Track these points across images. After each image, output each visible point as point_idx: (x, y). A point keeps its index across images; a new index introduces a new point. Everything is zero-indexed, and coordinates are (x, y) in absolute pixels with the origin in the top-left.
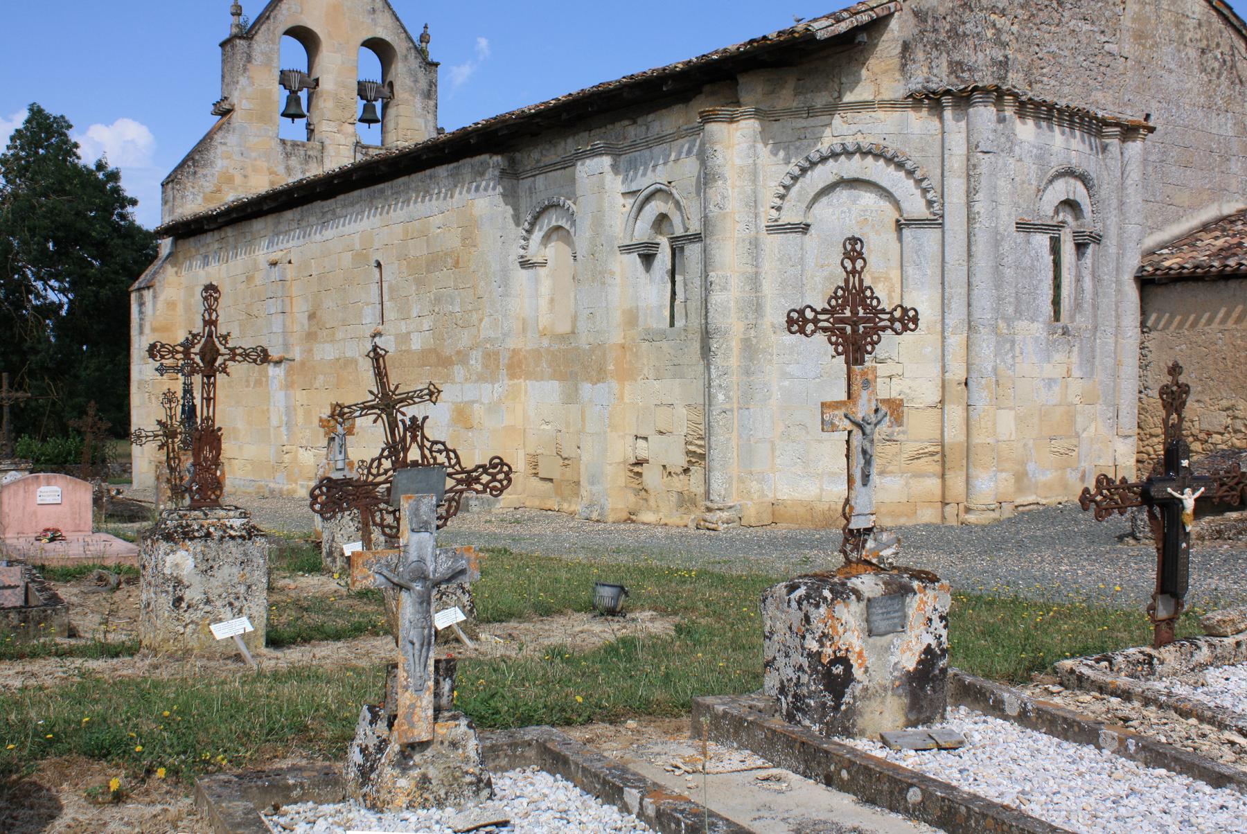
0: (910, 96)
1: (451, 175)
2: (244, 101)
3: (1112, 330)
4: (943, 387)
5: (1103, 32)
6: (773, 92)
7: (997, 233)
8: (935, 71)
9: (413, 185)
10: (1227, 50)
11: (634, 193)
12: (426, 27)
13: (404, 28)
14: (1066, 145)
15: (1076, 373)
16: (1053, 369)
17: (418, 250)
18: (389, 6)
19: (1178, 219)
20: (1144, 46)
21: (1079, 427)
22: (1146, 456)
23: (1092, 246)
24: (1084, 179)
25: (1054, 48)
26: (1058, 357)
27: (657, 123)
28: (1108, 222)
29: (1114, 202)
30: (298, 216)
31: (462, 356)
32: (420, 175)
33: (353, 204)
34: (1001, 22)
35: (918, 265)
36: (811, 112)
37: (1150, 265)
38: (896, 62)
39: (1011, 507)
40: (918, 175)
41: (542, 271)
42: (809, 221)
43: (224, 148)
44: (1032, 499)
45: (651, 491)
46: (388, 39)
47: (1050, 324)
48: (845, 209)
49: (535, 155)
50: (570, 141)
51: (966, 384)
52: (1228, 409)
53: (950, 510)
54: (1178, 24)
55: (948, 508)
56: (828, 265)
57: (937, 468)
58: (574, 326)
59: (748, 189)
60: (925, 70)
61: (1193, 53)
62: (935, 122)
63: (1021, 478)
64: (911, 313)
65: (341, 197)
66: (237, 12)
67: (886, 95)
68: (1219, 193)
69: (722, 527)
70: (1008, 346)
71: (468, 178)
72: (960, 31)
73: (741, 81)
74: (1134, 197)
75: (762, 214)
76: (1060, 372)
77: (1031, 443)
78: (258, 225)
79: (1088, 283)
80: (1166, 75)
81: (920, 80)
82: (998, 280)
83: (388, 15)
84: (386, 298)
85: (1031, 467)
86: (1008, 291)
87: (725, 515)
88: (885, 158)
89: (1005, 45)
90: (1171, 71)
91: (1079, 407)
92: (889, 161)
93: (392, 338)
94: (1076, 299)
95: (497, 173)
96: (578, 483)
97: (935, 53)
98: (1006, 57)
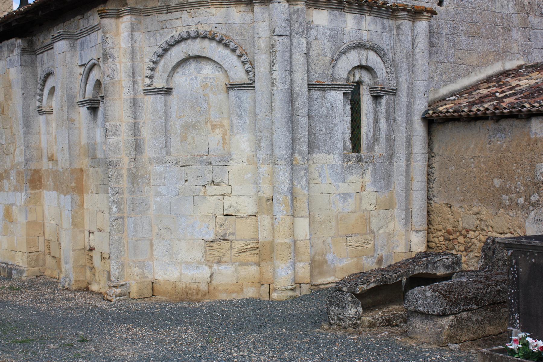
11: (84, 65)
15: (370, 188)
26: (351, 178)
28: (401, 80)
29: (404, 66)
35: (240, 116)
40: (238, 51)
41: (50, 117)
42: (171, 86)
45: (97, 269)
48: (193, 77)
51: (273, 200)
52: (477, 214)
56: (184, 117)
59: (129, 64)
68: (503, 54)
71: (6, 54)
75: (140, 82)
77: (329, 240)
79: (383, 124)
86: (303, 134)
87: (118, 291)
92: (220, 42)
95: (19, 51)
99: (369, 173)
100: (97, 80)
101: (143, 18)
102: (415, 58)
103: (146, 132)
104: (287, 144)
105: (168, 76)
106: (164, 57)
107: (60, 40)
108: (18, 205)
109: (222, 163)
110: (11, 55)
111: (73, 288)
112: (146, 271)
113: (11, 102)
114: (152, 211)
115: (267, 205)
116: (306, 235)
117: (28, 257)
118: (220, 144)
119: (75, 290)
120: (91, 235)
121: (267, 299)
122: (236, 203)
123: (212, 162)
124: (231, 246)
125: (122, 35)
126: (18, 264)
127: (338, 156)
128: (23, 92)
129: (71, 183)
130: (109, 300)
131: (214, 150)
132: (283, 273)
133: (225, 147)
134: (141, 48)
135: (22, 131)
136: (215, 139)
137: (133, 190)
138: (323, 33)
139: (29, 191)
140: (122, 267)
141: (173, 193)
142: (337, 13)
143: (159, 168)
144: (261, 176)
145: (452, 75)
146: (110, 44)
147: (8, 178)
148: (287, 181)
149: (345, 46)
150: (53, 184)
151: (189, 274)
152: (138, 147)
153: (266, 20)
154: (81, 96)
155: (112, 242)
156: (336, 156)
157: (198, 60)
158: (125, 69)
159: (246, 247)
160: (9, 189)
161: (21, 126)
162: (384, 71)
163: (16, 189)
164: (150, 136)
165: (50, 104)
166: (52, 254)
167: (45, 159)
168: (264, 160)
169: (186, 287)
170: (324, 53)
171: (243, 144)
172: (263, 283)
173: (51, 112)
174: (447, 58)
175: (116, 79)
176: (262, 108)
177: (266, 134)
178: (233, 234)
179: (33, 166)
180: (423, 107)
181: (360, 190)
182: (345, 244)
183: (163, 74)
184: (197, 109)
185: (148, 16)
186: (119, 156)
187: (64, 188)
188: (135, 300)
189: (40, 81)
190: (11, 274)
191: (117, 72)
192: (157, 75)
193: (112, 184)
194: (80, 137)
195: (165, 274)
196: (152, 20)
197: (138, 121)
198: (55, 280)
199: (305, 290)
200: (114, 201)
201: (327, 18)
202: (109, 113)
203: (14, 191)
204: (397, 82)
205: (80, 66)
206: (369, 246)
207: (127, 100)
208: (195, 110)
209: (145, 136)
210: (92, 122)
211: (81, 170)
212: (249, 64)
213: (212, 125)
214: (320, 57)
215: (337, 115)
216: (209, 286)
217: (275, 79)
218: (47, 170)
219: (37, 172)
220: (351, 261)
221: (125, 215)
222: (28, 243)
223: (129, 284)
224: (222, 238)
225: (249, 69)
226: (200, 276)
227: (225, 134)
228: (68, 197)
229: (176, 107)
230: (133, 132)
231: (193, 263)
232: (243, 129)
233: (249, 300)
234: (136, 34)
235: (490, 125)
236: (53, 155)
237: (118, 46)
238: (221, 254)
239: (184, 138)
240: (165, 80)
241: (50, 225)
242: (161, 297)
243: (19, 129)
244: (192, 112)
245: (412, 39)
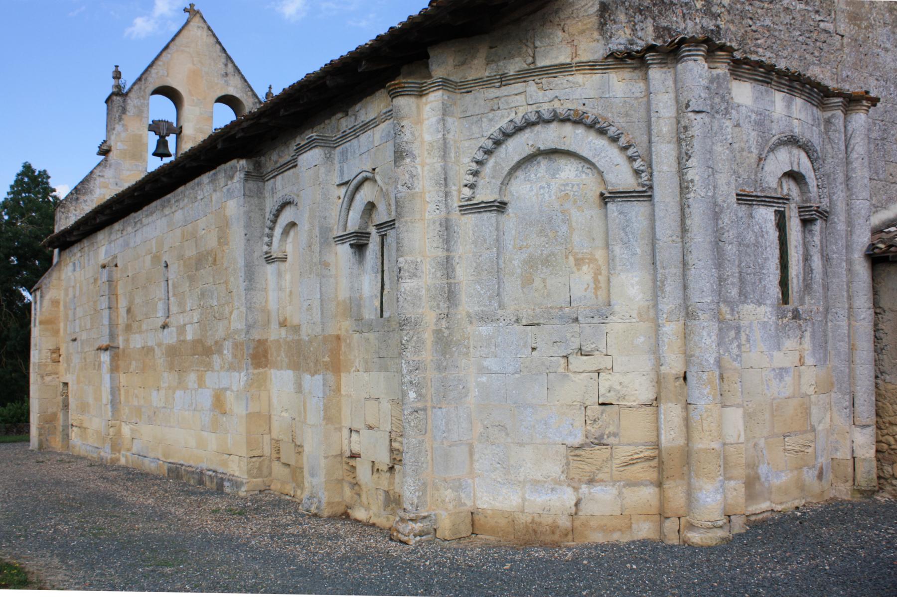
0: (612, 54)
1: (213, 181)
2: (119, 144)
3: (846, 312)
4: (658, 382)
5: (817, 12)
6: (463, 63)
7: (715, 204)
8: (640, 34)
12: (270, 88)
13: (250, 87)
14: (788, 111)
15: (810, 361)
16: (784, 358)
17: (191, 252)
18: (238, 71)
20: (859, 26)
21: (814, 420)
22: (885, 446)
23: (819, 222)
24: (807, 148)
25: (768, 22)
26: (790, 343)
27: (363, 111)
28: (835, 198)
29: (840, 177)
31: (219, 345)
32: (191, 184)
33: (152, 213)
35: (626, 244)
36: (503, 80)
37: (882, 242)
38: (595, 20)
39: (743, 519)
40: (623, 141)
41: (283, 266)
42: (505, 199)
43: (102, 179)
44: (765, 505)
45: (363, 487)
46: (238, 96)
47: (778, 308)
48: (544, 184)
49: (274, 157)
51: (685, 378)
53: (671, 525)
55: (667, 523)
57: (653, 475)
59: (438, 166)
60: (628, 31)
62: (642, 85)
63: (752, 483)
66: (117, 75)
67: (585, 57)
69: (413, 541)
70: (732, 334)
73: (431, 54)
74: (861, 173)
75: (455, 193)
76: (793, 358)
77: (762, 442)
79: (817, 263)
80: (882, 53)
81: (622, 41)
82: (719, 260)
83: (238, 78)
85: (763, 470)
86: (731, 271)
87: (418, 526)
88: (585, 125)
89: (716, 16)
90: (887, 50)
91: (813, 398)
92: (591, 126)
93: (174, 329)
94: (804, 280)
95: (242, 176)
97: (638, 17)
98: (718, 27)
99: (808, 334)
100: (369, 202)
101: (459, 96)
102: (850, 167)
103: (463, 273)
104: (712, 286)
105: (502, 184)
106: (495, 155)
107: (311, 149)
108: (235, 389)
109: (596, 320)
110: (229, 182)
111: (325, 514)
112: (463, 495)
113: (226, 247)
114: (473, 397)
115: (676, 387)
116: (739, 436)
117: (248, 463)
118: (589, 290)
119: (329, 517)
120: (353, 434)
121: (676, 542)
122: (621, 384)
123: (580, 318)
124: (611, 454)
125: (426, 122)
126: (232, 473)
127: (770, 309)
128: (246, 232)
129: (324, 356)
130: (401, 542)
131: (580, 298)
132: (708, 500)
133: (599, 293)
134: (455, 142)
135: (243, 285)
137: (444, 364)
138: (746, 117)
139: (250, 371)
140: (423, 488)
141: (511, 369)
142: (763, 88)
143: (485, 330)
144: (666, 340)
145: (884, 197)
146: (407, 136)
147: (220, 352)
148: (714, 346)
149: (775, 138)
150: (286, 360)
151: (539, 500)
152: (451, 295)
153: (669, 90)
154: (341, 228)
155: (408, 448)
156: (769, 309)
157: (553, 157)
158: (431, 174)
159: (636, 456)
160: (221, 368)
161: (241, 279)
162: (815, 183)
163: (232, 368)
164: (471, 278)
165: (283, 249)
166: (283, 460)
167: (274, 325)
168: (671, 313)
169: (533, 521)
170: (750, 147)
171: (631, 287)
172: (669, 514)
173: (284, 259)
174: (877, 174)
175: (417, 190)
176: (667, 227)
177: (673, 271)
178: (615, 435)
179: (256, 335)
180: (866, 239)
181: (797, 363)
182: (782, 449)
183: (494, 181)
184: (551, 234)
185: (468, 92)
186: (420, 311)
187: (312, 364)
188: (446, 542)
189: (268, 216)
190: (222, 486)
191: (418, 179)
192: (481, 182)
193: (409, 355)
194: (336, 289)
195: (494, 500)
196: (476, 99)
197: (452, 254)
198: (288, 497)
199: (739, 525)
200: (411, 382)
201: (751, 94)
202: (406, 242)
203: (228, 370)
205: (339, 185)
206: (810, 450)
207: (434, 222)
208: (546, 236)
209: (461, 278)
210: (356, 266)
211: (338, 338)
213: (576, 260)
214: (744, 154)
215: (768, 244)
216: (573, 520)
217: (692, 181)
218: (278, 341)
219: (261, 343)
220: (790, 475)
221: (429, 404)
222: (249, 443)
223: (435, 515)
224: (596, 441)
225: (642, 168)
226: (558, 504)
227: (598, 272)
228: (319, 378)
229: (513, 232)
230: (445, 272)
231: (545, 482)
232: (632, 264)
233: (644, 543)
234: (450, 120)
236: (285, 320)
237: (419, 139)
238: (594, 468)
239: (527, 281)
240: (497, 190)
241: (281, 418)
242: (488, 537)
243: (238, 283)
244: (543, 239)
245: (846, 140)
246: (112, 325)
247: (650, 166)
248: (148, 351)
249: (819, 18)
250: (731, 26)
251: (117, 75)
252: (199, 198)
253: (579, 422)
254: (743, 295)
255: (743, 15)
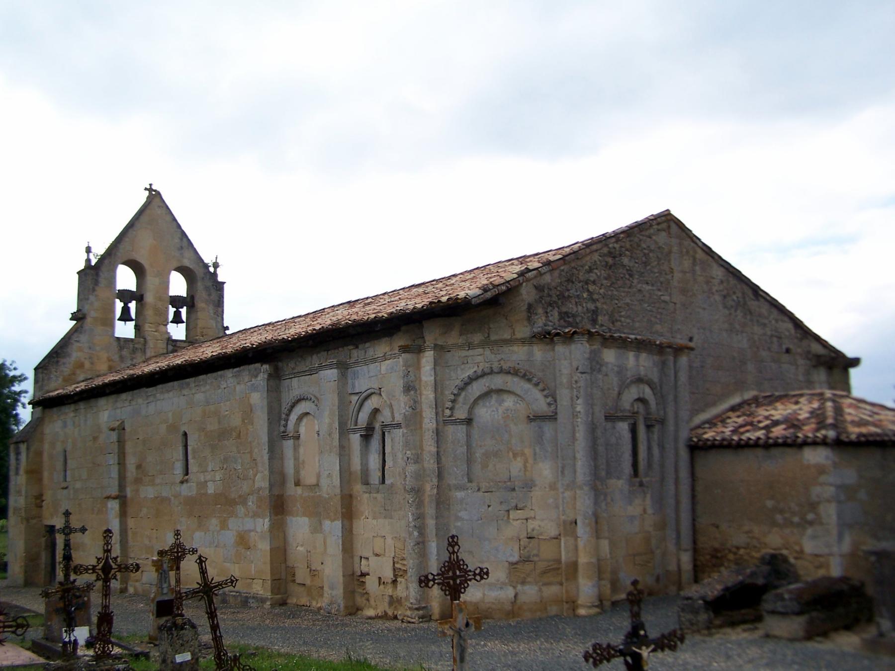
5: (659, 290)
9: (209, 381)
10: (740, 295)
14: (639, 363)
15: (650, 511)
16: (635, 509)
17: (212, 426)
19: (714, 404)
24: (650, 383)
25: (628, 300)
26: (637, 501)
30: (130, 398)
31: (243, 500)
33: (168, 391)
34: (591, 288)
36: (470, 346)
43: (78, 344)
49: (292, 364)
50: (314, 357)
52: (747, 532)
54: (707, 282)
58: (318, 481)
60: (544, 318)
61: (717, 298)
64: (485, 570)
65: (160, 386)
66: (88, 250)
67: (519, 335)
68: (740, 386)
70: (602, 497)
72: (567, 294)
78: (102, 402)
79: (656, 451)
84: (190, 457)
90: (704, 309)
93: (194, 484)
95: (266, 376)
96: (322, 588)
97: (550, 308)
98: (596, 307)
99: (648, 496)
136: (516, 467)
141: (475, 518)
163: (255, 515)
171: (545, 471)
178: (537, 555)
204: (665, 412)
212: (552, 396)
227: (526, 461)
234: (438, 368)
235: (760, 452)
240: (466, 412)
246: (122, 478)
247: (556, 401)
248: (161, 500)
249: (660, 293)
250: (605, 306)
251: (88, 250)
252: (222, 387)
253: (516, 548)
254: (609, 474)
255: (612, 298)
